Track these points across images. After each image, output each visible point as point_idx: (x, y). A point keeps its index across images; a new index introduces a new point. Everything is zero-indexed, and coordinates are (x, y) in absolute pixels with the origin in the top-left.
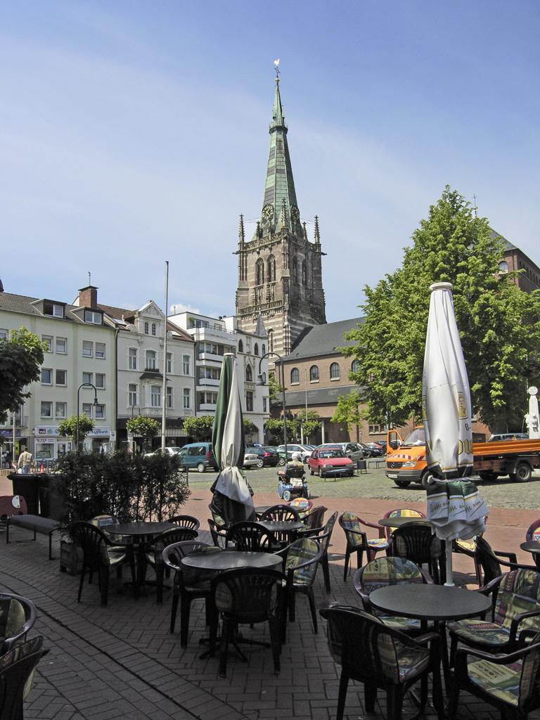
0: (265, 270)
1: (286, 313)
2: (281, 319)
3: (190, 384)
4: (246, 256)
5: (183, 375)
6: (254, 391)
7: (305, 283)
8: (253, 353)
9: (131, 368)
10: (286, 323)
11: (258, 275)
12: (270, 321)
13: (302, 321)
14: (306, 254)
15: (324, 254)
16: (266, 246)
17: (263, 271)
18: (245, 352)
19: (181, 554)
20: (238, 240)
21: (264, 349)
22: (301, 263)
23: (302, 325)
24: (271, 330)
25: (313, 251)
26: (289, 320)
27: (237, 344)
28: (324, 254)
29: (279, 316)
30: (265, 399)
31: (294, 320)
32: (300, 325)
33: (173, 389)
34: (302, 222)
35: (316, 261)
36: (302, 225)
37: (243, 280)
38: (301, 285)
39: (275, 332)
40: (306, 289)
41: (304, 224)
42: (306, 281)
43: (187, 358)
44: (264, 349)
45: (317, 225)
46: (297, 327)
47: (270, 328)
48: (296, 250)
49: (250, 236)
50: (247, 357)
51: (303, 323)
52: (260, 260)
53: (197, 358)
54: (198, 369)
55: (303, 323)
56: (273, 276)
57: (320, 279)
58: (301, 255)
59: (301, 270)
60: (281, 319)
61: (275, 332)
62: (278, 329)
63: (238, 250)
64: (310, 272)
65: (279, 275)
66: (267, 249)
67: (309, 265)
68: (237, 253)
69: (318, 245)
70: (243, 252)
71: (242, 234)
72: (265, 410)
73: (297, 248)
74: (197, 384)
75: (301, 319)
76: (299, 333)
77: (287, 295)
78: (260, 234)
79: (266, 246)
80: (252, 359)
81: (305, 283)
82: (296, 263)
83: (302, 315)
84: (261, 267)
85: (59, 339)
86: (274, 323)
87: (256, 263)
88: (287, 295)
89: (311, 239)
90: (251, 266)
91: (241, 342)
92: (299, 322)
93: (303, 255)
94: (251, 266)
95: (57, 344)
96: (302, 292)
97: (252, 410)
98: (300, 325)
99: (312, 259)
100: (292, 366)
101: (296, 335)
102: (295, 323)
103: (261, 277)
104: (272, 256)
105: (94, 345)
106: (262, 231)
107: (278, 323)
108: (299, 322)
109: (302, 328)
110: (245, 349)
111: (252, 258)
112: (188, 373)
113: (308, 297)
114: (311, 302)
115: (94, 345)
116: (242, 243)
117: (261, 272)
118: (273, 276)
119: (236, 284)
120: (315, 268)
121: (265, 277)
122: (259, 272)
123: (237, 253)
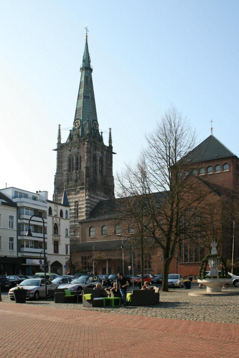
0: (74, 162)
2: (84, 195)
3: (14, 235)
5: (9, 228)
6: (59, 240)
7: (101, 172)
8: (59, 216)
9: (10, 227)
10: (87, 198)
11: (69, 165)
13: (98, 196)
14: (102, 153)
17: (73, 163)
18: (53, 215)
21: (67, 213)
22: (98, 159)
23: (98, 199)
24: (77, 201)
25: (107, 151)
26: (89, 196)
27: (47, 210)
29: (83, 193)
30: (67, 246)
31: (93, 196)
32: (97, 199)
33: (2, 237)
34: (100, 131)
36: (100, 134)
38: (98, 173)
39: (80, 203)
40: (102, 175)
41: (102, 133)
43: (11, 217)
44: (67, 213)
47: (77, 200)
48: (95, 149)
50: (55, 219)
51: (99, 198)
53: (19, 217)
54: (19, 225)
55: (99, 198)
56: (79, 166)
58: (99, 153)
59: (98, 163)
61: (80, 203)
62: (83, 201)
63: (56, 148)
64: (104, 164)
67: (105, 160)
68: (55, 150)
69: (111, 147)
71: (59, 137)
72: (67, 253)
73: (96, 148)
74: (19, 234)
75: (98, 195)
76: (96, 204)
77: (88, 179)
78: (71, 137)
80: (58, 220)
81: (101, 172)
82: (95, 159)
83: (98, 193)
85: (161, 285)
86: (79, 197)
87: (68, 157)
89: (106, 143)
91: (50, 209)
92: (96, 197)
95: (45, 244)
96: (99, 177)
97: (58, 253)
98: (97, 199)
99: (106, 156)
101: (94, 205)
102: (93, 198)
103: (71, 166)
104: (78, 153)
105: (29, 247)
106: (73, 136)
108: (96, 197)
109: (98, 201)
110: (54, 213)
112: (12, 227)
113: (103, 181)
115: (29, 247)
116: (59, 143)
117: (71, 163)
118: (79, 166)
121: (74, 167)
122: (70, 163)
123: (55, 150)
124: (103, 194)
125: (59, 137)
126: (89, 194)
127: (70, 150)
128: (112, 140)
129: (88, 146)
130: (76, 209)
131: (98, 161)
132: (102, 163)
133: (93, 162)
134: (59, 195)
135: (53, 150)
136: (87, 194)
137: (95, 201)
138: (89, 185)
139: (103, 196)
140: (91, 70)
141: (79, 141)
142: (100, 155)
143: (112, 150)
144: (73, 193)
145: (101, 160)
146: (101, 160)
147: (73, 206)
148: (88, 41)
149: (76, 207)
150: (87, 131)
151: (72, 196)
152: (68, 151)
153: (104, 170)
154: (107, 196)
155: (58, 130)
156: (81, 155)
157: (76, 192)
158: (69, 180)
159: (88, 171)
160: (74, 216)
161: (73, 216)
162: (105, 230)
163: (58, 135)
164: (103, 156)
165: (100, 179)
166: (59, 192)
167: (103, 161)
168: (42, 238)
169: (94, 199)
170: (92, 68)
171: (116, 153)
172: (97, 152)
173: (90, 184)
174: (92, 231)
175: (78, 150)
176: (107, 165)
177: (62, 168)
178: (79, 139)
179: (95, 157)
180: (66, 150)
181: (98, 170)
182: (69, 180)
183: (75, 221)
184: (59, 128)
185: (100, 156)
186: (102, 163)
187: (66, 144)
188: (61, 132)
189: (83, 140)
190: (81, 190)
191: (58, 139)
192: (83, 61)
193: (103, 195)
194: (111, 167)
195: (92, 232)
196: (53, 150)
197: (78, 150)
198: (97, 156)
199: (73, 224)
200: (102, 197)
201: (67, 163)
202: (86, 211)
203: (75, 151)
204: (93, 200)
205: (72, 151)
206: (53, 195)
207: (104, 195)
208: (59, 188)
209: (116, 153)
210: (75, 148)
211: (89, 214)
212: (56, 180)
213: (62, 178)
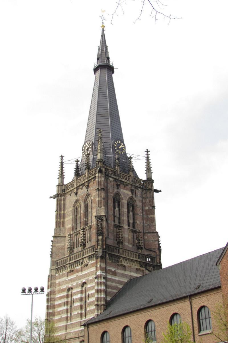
1: (99, 259)
2: (94, 269)
4: (64, 200)
10: (99, 273)
12: (84, 272)
15: (157, 191)
16: (83, 185)
19: (208, 325)
20: (57, 182)
23: (125, 276)
24: (85, 283)
28: (157, 191)
29: (93, 265)
31: (113, 269)
35: (148, 200)
37: (60, 227)
38: (126, 227)
42: (134, 223)
45: (148, 159)
46: (116, 278)
49: (69, 177)
51: (127, 273)
52: (77, 201)
55: (127, 273)
57: (153, 220)
58: (125, 193)
59: (125, 210)
60: (94, 269)
64: (139, 211)
65: (93, 213)
66: (84, 188)
67: (139, 204)
68: (54, 197)
69: (150, 181)
70: (61, 195)
71: (62, 175)
73: (118, 184)
76: (120, 286)
78: (78, 173)
79: (83, 185)
82: (119, 203)
83: (125, 263)
84: (79, 209)
87: (74, 206)
88: (100, 237)
89: (142, 176)
90: (69, 210)
93: (130, 193)
94: (69, 210)
96: (127, 235)
98: (122, 275)
100: (142, 318)
104: (88, 195)
107: (90, 274)
108: (120, 271)
109: (126, 280)
111: (70, 199)
114: (139, 247)
116: (61, 185)
119: (51, 232)
120: (147, 208)
123: (54, 197)
124: (137, 266)
125: (62, 175)
126: (103, 265)
127: (76, 194)
128: (151, 169)
129: (100, 179)
130: (84, 299)
131: (126, 206)
132: (133, 209)
133: (114, 208)
134: (57, 275)
135: (51, 198)
136: (98, 266)
137: (113, 282)
138: (103, 249)
139: (137, 269)
140: (111, 69)
141: (88, 175)
142: (127, 194)
143: (152, 186)
144: (78, 268)
145: (131, 205)
146: (131, 205)
147: (79, 294)
148: (105, 32)
149: (84, 296)
150: (99, 155)
151: (77, 274)
152: (73, 195)
153: (138, 222)
154: (146, 269)
155: (60, 164)
156: (93, 199)
157: (83, 265)
158: (75, 246)
159: (101, 224)
160: (79, 312)
161: (78, 314)
162: (206, 319)
163: (59, 172)
164: (134, 196)
165: (130, 238)
166: (58, 270)
167: (137, 206)
168: (205, 317)
169: (116, 275)
170: (111, 65)
171: (160, 191)
172: (122, 190)
173: (104, 247)
174: (127, 335)
175: (88, 191)
176: (144, 213)
177: (63, 226)
178: (88, 172)
179: (117, 200)
180: (71, 195)
181: (126, 222)
182: (75, 246)
183: (66, 326)
184: (60, 161)
185: (128, 198)
186: (133, 209)
187: (71, 184)
188: (63, 166)
189: (94, 172)
190: (90, 261)
191: (58, 178)
192: (98, 59)
193: (137, 267)
194: (152, 216)
195: (204, 321)
196: (51, 198)
197: (88, 191)
198: (123, 197)
199: (77, 330)
200: (134, 272)
201: (71, 217)
202: (98, 299)
203: (84, 192)
204: (113, 278)
205: (79, 193)
206: (49, 275)
207: (139, 267)
208: (58, 263)
209: (160, 191)
210: (83, 188)
211: (103, 305)
212: (55, 248)
213: (63, 244)
